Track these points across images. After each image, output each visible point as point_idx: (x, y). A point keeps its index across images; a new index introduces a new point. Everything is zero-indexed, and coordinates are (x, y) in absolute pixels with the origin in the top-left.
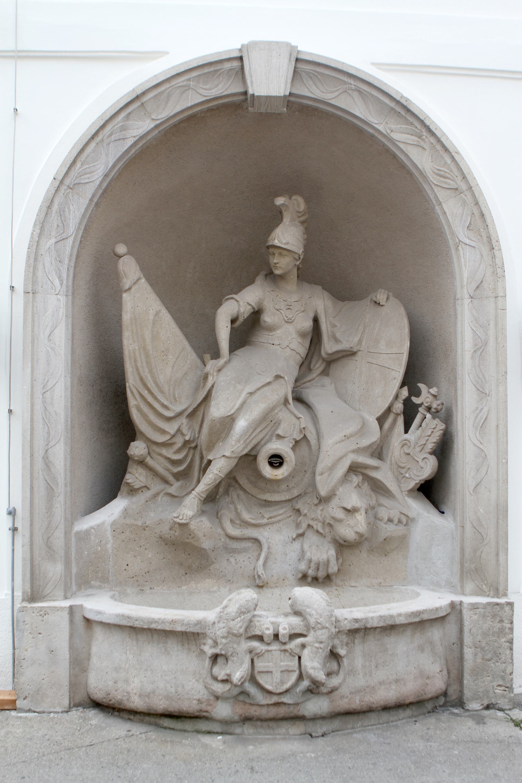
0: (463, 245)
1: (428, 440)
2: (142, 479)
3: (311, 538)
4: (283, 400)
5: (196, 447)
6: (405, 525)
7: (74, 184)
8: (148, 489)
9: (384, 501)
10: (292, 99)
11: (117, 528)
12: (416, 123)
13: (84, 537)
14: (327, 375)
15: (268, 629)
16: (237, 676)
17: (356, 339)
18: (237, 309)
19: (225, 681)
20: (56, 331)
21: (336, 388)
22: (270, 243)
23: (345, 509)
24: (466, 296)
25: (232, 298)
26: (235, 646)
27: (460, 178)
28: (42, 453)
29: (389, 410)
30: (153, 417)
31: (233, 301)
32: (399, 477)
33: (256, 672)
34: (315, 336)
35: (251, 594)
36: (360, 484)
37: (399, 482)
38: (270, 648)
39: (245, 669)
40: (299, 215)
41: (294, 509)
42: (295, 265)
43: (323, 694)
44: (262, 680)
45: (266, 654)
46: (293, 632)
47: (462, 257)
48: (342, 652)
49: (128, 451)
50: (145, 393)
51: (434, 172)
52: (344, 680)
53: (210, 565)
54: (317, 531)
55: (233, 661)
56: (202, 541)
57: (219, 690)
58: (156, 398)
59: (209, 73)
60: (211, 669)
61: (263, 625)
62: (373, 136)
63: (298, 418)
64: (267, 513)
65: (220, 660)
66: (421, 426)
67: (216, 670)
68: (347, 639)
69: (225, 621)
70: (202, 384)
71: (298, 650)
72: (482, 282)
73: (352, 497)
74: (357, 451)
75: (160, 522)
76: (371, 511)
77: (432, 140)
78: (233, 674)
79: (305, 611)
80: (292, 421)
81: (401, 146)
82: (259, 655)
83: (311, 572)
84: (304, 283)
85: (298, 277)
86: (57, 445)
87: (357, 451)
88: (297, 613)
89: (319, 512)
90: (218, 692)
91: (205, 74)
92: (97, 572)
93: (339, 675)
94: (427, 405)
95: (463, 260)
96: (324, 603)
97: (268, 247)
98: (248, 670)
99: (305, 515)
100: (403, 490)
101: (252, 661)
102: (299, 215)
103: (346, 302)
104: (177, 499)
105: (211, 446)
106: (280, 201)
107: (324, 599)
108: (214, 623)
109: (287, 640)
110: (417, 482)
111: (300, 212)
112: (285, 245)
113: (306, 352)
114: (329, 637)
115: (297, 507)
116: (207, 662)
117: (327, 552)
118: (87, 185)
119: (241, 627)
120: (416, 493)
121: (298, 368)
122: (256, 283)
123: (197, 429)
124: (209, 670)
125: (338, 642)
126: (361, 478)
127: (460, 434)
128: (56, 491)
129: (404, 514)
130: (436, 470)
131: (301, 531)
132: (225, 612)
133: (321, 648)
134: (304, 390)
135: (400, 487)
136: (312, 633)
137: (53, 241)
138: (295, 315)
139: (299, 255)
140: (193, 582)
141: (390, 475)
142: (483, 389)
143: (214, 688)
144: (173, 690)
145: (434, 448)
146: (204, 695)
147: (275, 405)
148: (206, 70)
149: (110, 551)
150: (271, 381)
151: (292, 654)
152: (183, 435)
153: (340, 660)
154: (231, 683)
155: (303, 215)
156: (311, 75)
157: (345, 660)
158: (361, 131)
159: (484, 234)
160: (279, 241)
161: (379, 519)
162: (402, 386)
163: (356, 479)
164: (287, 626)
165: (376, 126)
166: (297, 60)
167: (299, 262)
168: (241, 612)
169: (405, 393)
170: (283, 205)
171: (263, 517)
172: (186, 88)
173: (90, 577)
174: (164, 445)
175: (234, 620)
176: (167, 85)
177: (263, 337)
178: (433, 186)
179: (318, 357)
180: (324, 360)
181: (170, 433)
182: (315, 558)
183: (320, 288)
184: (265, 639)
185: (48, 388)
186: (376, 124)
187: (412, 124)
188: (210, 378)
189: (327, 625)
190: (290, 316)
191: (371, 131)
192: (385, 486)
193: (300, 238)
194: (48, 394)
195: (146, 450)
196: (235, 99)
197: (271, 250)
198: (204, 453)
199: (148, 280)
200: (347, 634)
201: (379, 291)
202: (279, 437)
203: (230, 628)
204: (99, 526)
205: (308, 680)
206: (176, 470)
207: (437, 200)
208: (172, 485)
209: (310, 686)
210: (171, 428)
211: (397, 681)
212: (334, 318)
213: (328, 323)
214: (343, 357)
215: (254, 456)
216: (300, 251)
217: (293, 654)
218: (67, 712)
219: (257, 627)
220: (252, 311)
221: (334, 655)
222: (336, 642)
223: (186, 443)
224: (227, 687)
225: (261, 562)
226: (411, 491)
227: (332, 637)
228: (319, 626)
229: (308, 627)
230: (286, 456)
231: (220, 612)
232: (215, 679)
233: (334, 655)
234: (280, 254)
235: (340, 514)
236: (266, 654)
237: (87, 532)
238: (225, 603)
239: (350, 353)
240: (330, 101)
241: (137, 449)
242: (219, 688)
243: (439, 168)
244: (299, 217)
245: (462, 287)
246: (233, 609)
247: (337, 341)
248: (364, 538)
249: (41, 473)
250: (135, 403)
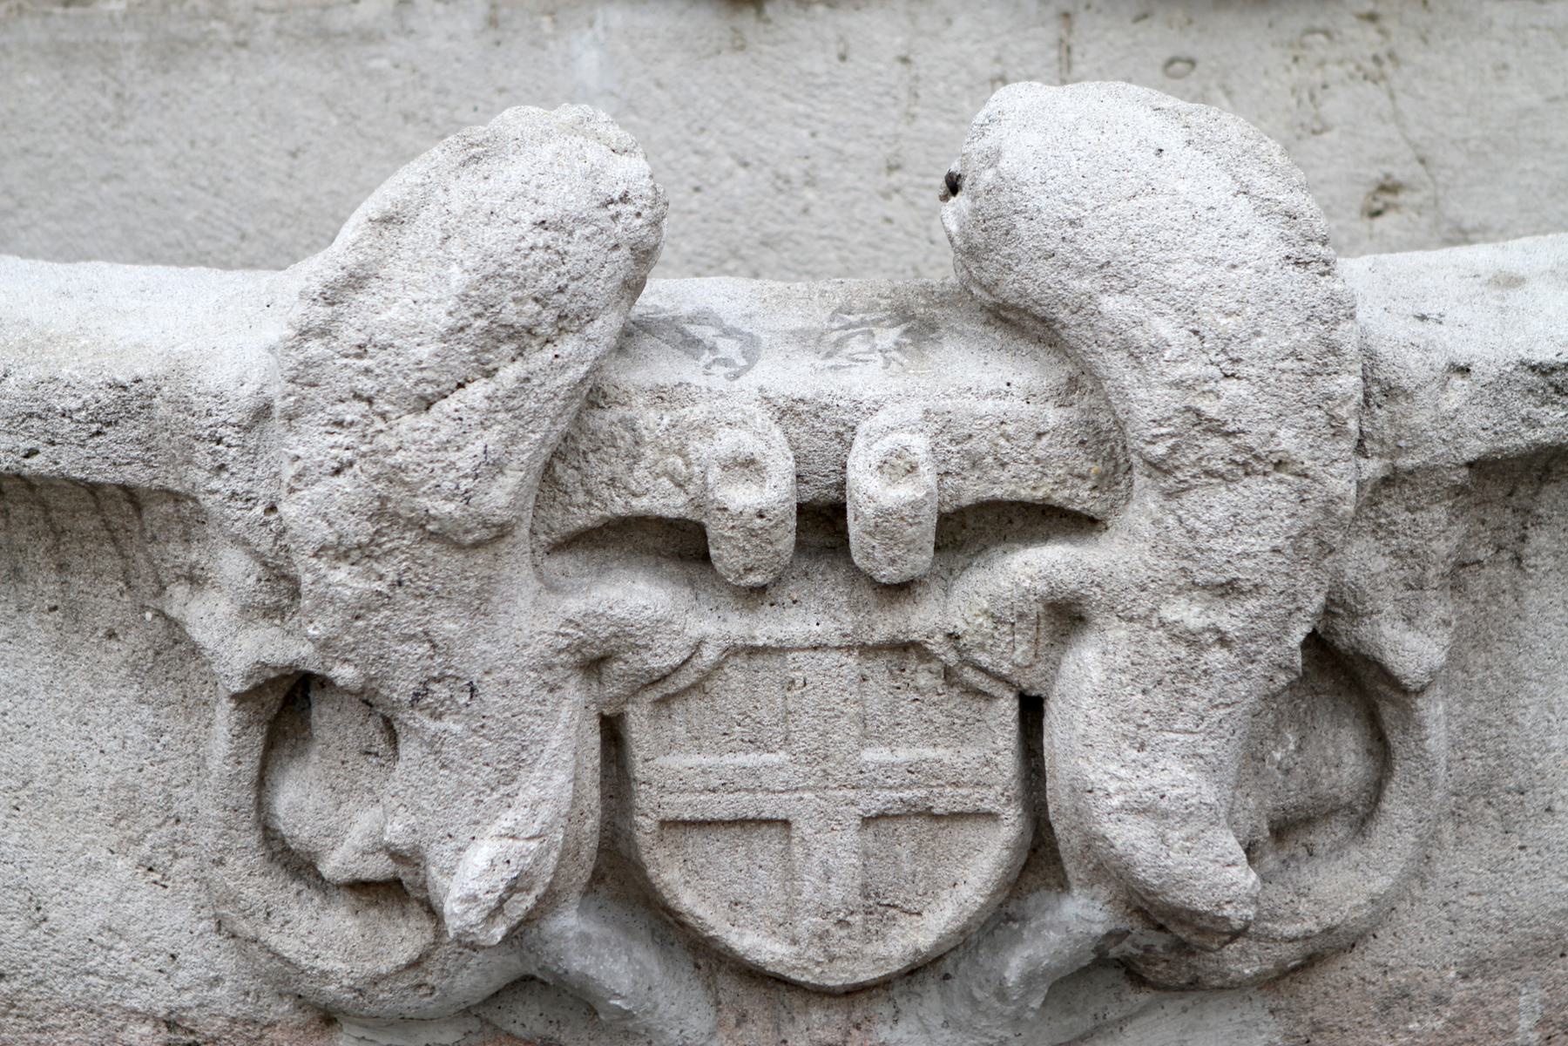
15: (748, 465)
16: (474, 873)
26: (448, 626)
33: (646, 823)
35: (595, 154)
38: (765, 627)
39: (545, 812)
43: (1235, 988)
44: (692, 886)
45: (736, 675)
46: (973, 490)
48: (1411, 648)
52: (1420, 870)
55: (434, 745)
57: (332, 962)
60: (262, 782)
61: (706, 429)
67: (299, 798)
68: (1460, 529)
69: (352, 411)
71: (1021, 653)
78: (438, 855)
79: (1084, 307)
82: (669, 689)
88: (1019, 321)
93: (1380, 831)
96: (1265, 242)
98: (574, 816)
101: (613, 732)
107: (1266, 208)
108: (263, 412)
109: (921, 560)
114: (1296, 541)
116: (223, 737)
119: (493, 467)
124: (247, 797)
125: (1380, 564)
132: (350, 335)
133: (1223, 641)
136: (1143, 508)
143: (289, 946)
146: (217, 980)
151: (962, 676)
153: (1388, 713)
154: (433, 912)
157: (1434, 712)
164: (919, 445)
168: (492, 334)
175: (427, 404)
184: (726, 556)
189: (1287, 440)
200: (1459, 490)
203: (394, 476)
205: (1103, 892)
209: (1115, 936)
217: (970, 675)
219: (650, 454)
221: (1340, 672)
222: (1364, 560)
224: (403, 939)
227: (1316, 543)
228: (1215, 451)
229: (1110, 452)
231: (304, 334)
232: (297, 865)
233: (1340, 672)
236: (736, 675)
238: (349, 242)
246: (416, 305)
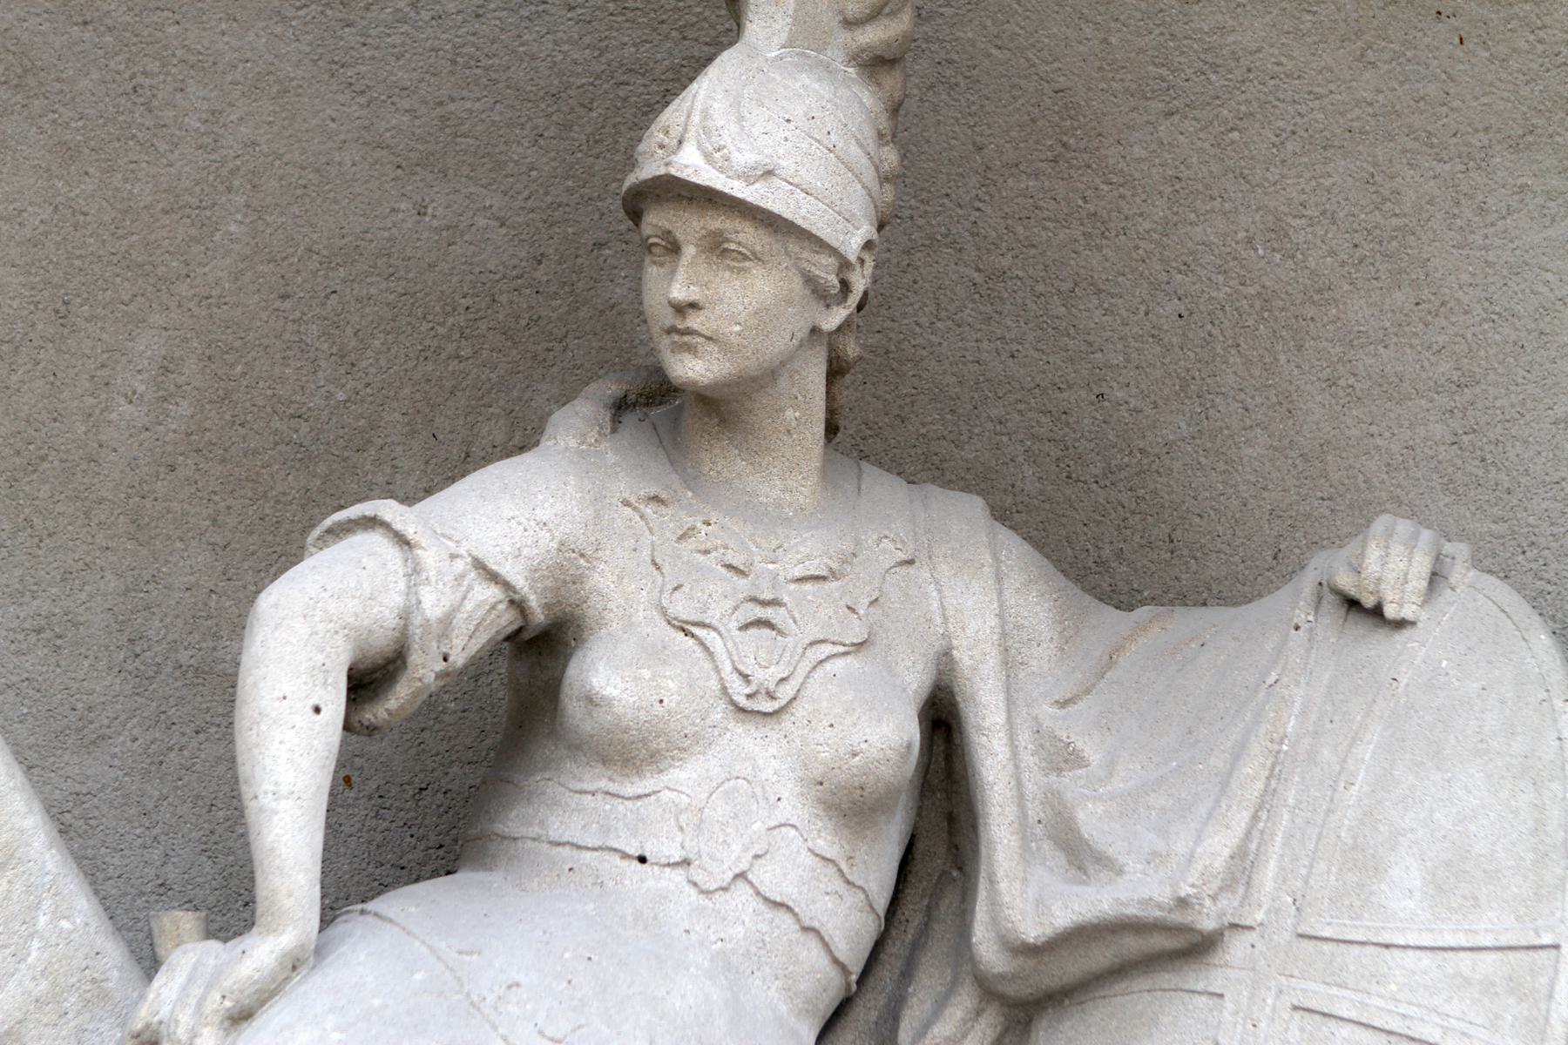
17: (1219, 845)
18: (395, 599)
22: (648, 170)
25: (371, 523)
31: (374, 541)
34: (934, 810)
42: (815, 331)
84: (870, 471)
85: (831, 429)
97: (637, 202)
103: (1143, 612)
112: (748, 177)
113: (867, 928)
122: (546, 443)
138: (804, 667)
139: (844, 265)
160: (708, 157)
177: (571, 811)
180: (988, 991)
183: (975, 506)
190: (766, 676)
193: (855, 149)
197: (656, 220)
201: (1380, 524)
212: (1063, 704)
213: (1025, 738)
214: (1121, 971)
216: (853, 238)
218: (1234, 926)
220: (506, 620)
234: (716, 247)
247: (1080, 856)
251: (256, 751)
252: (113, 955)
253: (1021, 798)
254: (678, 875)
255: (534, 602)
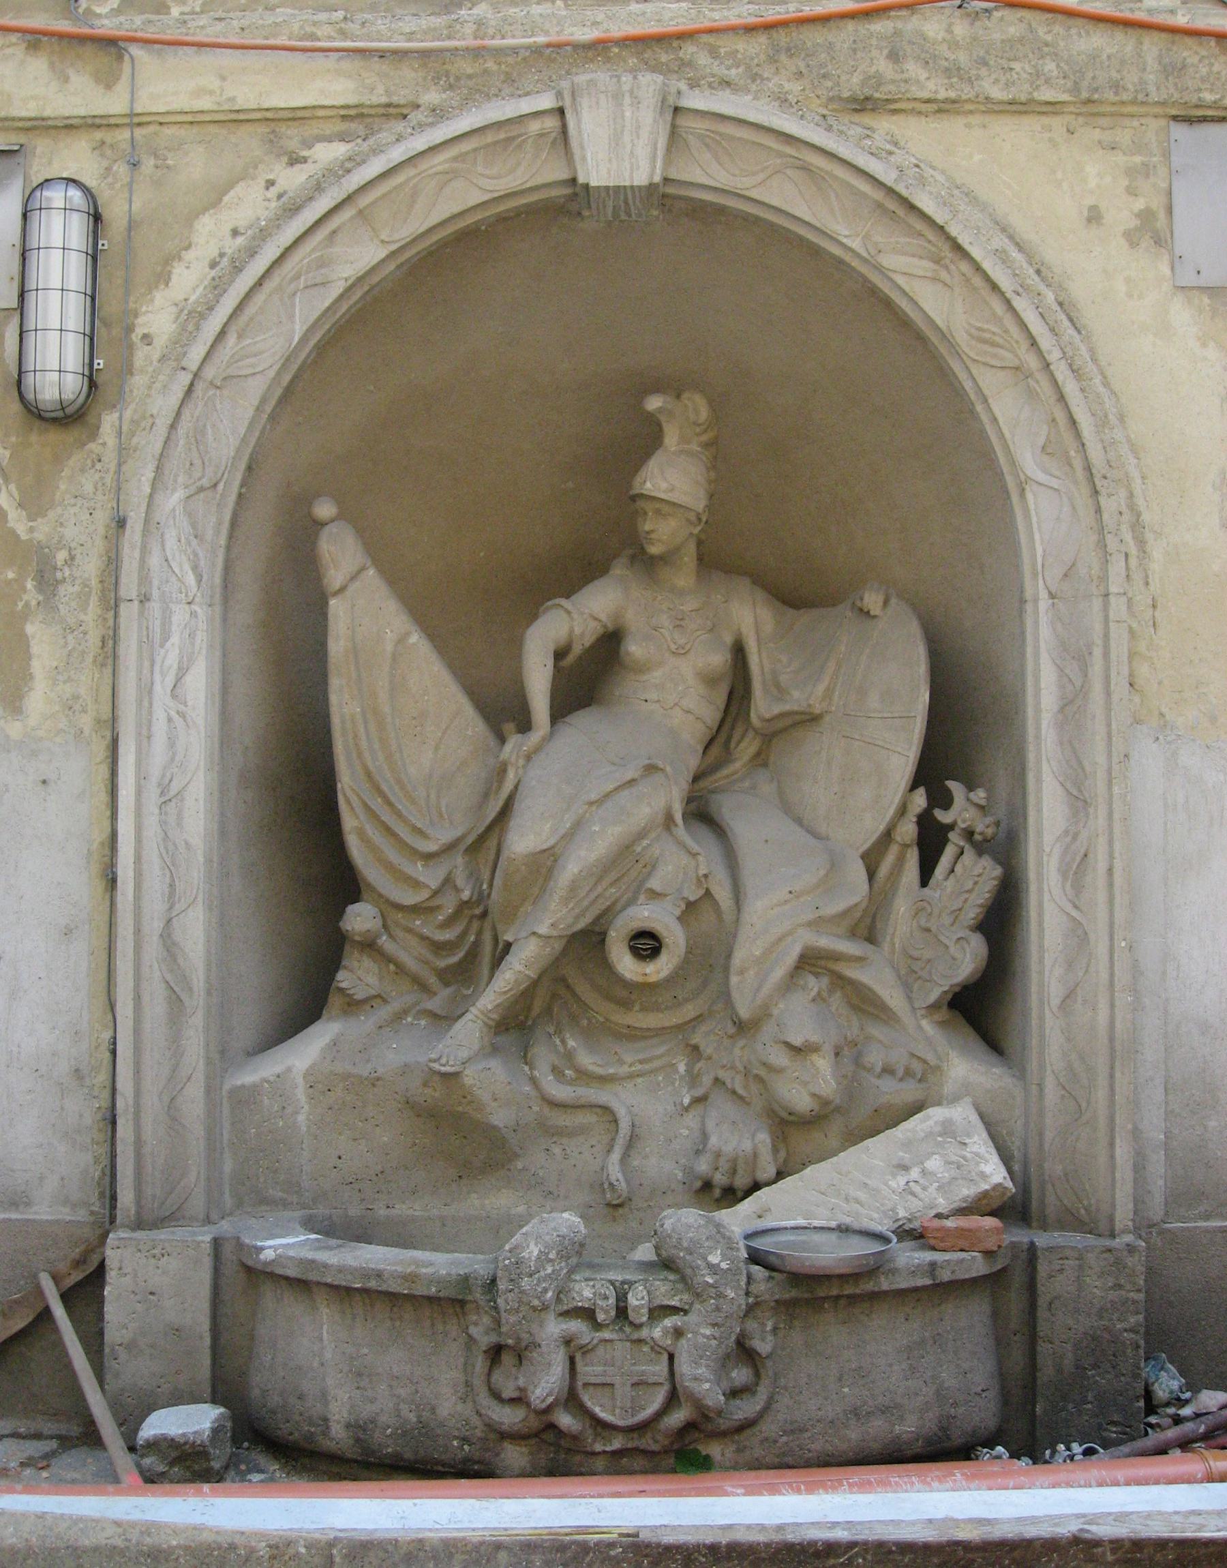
0: (1035, 487)
1: (966, 900)
2: (372, 979)
3: (721, 1107)
4: (660, 818)
5: (484, 914)
6: (920, 1081)
7: (225, 379)
8: (385, 1001)
9: (876, 1031)
10: (671, 190)
11: (318, 1083)
12: (930, 234)
13: (244, 1099)
14: (765, 765)
19: (519, 1400)
20: (188, 678)
21: (781, 794)
23: (788, 1045)
24: (1043, 594)
27: (1025, 344)
28: (158, 925)
29: (887, 836)
30: (393, 855)
32: (909, 980)
33: (580, 1383)
36: (825, 994)
37: (907, 987)
40: (698, 430)
41: (688, 1045)
47: (1033, 513)
48: (763, 1346)
49: (341, 924)
50: (377, 804)
51: (970, 335)
53: (510, 1161)
54: (734, 1092)
56: (488, 1110)
58: (399, 814)
59: (495, 143)
60: (489, 1374)
62: (841, 262)
63: (694, 855)
64: (630, 1056)
65: (507, 1359)
66: (953, 871)
70: (495, 784)
72: (1074, 564)
73: (800, 1017)
74: (817, 924)
75: (406, 1069)
76: (849, 1053)
77: (964, 267)
80: (679, 863)
81: (901, 280)
82: (586, 1350)
83: (720, 1179)
86: (190, 910)
87: (817, 924)
89: (737, 1051)
90: (502, 1423)
91: (488, 145)
92: (276, 1171)
94: (963, 826)
95: (1034, 520)
97: (634, 498)
99: (710, 1058)
100: (917, 1005)
101: (572, 1360)
102: (698, 430)
104: (444, 1020)
105: (511, 914)
106: (654, 403)
110: (946, 988)
111: (699, 425)
113: (719, 716)
115: (693, 1042)
117: (753, 1136)
118: (250, 379)
120: (944, 1014)
121: (700, 749)
123: (486, 875)
126: (825, 981)
127: (1033, 888)
128: (187, 1004)
129: (919, 1058)
130: (984, 963)
131: (699, 1092)
134: (713, 796)
135: (910, 999)
137: (179, 494)
140: (474, 1195)
141: (888, 974)
142: (1080, 791)
144: (412, 1417)
145: (981, 916)
147: (644, 829)
148: (490, 138)
149: (304, 1129)
150: (636, 776)
151: (656, 1348)
152: (458, 890)
154: (528, 1405)
155: (705, 431)
156: (707, 140)
158: (815, 252)
159: (1078, 463)
161: (864, 1068)
162: (913, 787)
163: (813, 984)
165: (845, 241)
166: (677, 110)
167: (699, 528)
169: (920, 800)
170: (660, 410)
171: (621, 1062)
172: (451, 175)
173: (262, 1180)
174: (415, 910)
176: (410, 172)
178: (968, 362)
179: (741, 729)
181: (428, 886)
182: (728, 1149)
185: (172, 793)
186: (846, 237)
187: (920, 235)
188: (511, 775)
191: (837, 251)
192: (879, 997)
194: (171, 808)
195: (379, 922)
196: (554, 193)
198: (499, 927)
199: (381, 571)
202: (654, 895)
204: (278, 1076)
206: (442, 963)
207: (979, 390)
208: (435, 994)
210: (431, 877)
211: (884, 1410)
214: (795, 725)
215: (600, 934)
216: (700, 505)
220: (600, 631)
221: (744, 1352)
223: (463, 906)
225: (616, 1156)
226: (934, 1007)
230: (665, 934)
233: (744, 1352)
234: (658, 512)
235: (779, 1058)
237: (255, 1089)
239: (808, 717)
240: (747, 193)
241: (360, 918)
242: (509, 1417)
243: (979, 325)
244: (699, 435)
245: (1035, 575)
248: (831, 1107)
249: (156, 966)
250: (355, 823)
251: (283, 1461)
252: (492, 741)
253: (763, 673)
254: (658, 705)
255: (609, 625)
